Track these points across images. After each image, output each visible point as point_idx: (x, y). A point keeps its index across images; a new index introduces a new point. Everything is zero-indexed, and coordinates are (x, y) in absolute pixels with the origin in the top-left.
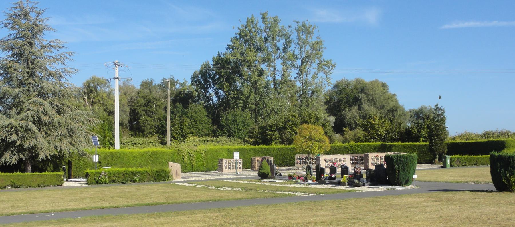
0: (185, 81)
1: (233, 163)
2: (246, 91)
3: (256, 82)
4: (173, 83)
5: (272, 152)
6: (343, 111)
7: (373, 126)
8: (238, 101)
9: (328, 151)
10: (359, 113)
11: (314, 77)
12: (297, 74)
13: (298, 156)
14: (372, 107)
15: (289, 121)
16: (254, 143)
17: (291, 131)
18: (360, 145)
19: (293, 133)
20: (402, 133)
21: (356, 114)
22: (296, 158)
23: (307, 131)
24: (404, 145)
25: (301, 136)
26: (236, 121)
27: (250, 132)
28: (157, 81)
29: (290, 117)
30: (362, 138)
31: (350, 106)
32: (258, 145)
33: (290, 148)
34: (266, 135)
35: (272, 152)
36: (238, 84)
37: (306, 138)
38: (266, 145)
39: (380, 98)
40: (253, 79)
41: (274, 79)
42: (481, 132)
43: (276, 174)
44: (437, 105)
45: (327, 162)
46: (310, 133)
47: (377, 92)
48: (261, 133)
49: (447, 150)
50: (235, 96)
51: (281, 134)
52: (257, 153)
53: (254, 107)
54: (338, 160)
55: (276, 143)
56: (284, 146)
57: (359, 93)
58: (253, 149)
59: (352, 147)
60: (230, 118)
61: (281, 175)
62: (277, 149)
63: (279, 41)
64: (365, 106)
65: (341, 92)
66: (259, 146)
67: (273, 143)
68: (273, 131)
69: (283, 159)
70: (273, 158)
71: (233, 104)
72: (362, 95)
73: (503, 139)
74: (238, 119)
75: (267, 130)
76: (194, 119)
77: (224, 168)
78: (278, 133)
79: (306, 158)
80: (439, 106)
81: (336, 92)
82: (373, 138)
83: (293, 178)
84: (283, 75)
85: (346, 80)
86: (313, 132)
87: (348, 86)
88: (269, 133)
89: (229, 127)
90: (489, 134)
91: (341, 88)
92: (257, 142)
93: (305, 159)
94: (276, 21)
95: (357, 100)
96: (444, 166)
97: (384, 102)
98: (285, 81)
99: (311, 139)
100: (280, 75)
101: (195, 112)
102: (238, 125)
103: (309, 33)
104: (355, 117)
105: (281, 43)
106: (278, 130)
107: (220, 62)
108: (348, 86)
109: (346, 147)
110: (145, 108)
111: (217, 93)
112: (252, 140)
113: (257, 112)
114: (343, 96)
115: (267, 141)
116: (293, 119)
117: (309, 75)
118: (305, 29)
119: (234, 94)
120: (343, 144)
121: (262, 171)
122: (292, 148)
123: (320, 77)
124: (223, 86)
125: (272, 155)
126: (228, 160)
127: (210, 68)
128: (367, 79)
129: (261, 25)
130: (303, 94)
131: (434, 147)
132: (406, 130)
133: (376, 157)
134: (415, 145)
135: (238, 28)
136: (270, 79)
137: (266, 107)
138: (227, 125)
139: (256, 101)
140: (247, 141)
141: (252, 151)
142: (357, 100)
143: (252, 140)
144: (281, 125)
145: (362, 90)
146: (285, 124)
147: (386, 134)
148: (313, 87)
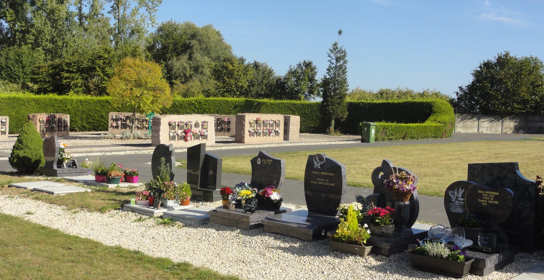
2: (38, 22)
3: (52, 12)
5: (69, 107)
6: (169, 60)
7: (231, 74)
8: (27, 36)
9: (168, 107)
10: (190, 64)
11: (135, 12)
13: (113, 115)
14: (206, 57)
15: (100, 57)
16: (38, 92)
17: (102, 75)
18: (212, 101)
19: (106, 78)
20: (271, 86)
21: (185, 65)
22: (110, 117)
23: (133, 71)
24: (279, 104)
25: (121, 79)
26: (21, 62)
27: (33, 73)
29: (102, 52)
30: (213, 90)
31: (178, 54)
32: (45, 93)
33: (99, 101)
35: (69, 107)
37: (130, 82)
38: (60, 94)
39: (215, 47)
40: (49, 7)
41: (80, 9)
42: (376, 91)
43: (60, 163)
44: (335, 44)
45: (174, 128)
46: (138, 74)
47: (212, 39)
48: (53, 76)
49: (347, 113)
50: (24, 29)
51: (86, 79)
52: (42, 107)
53: (50, 46)
54: (193, 124)
55: (77, 93)
56: (89, 97)
57: (189, 39)
58: (34, 100)
60: (12, 57)
61: (74, 164)
62: (77, 101)
64: (197, 55)
65: (167, 36)
66: (46, 96)
67: (72, 92)
68: (73, 72)
69: (87, 118)
70: (69, 116)
71: (19, 39)
72: (194, 42)
73: (428, 101)
74: (24, 59)
75: (63, 70)
78: (80, 77)
79: (127, 118)
80: (339, 46)
81: (161, 36)
82: (230, 92)
83: (110, 180)
84: (92, 6)
85: (173, 22)
86: (144, 73)
87: (175, 30)
88: (66, 75)
89: (11, 70)
90: (387, 94)
91: (166, 32)
92: (45, 89)
93: (126, 121)
95: (186, 48)
96: (365, 140)
97: (221, 52)
98: (95, 14)
99: (139, 84)
100: (89, 6)
102: (23, 67)
104: (185, 69)
106: (81, 71)
108: (175, 30)
109: (190, 104)
112: (36, 87)
113: (53, 53)
114: (169, 41)
115: (61, 89)
116: (106, 56)
117: (127, 9)
119: (21, 26)
120: (184, 99)
121: (21, 154)
122: (103, 101)
123: (141, 14)
124: (5, 14)
125: (64, 112)
128: (199, 24)
130: (119, 33)
131: (330, 107)
132: (277, 82)
133: (257, 122)
134: (294, 104)
136: (73, 9)
137: (66, 46)
138: (8, 67)
140: (28, 88)
142: (186, 48)
143: (36, 87)
144: (86, 64)
145: (193, 36)
146: (93, 62)
147: (249, 86)
148: (133, 25)
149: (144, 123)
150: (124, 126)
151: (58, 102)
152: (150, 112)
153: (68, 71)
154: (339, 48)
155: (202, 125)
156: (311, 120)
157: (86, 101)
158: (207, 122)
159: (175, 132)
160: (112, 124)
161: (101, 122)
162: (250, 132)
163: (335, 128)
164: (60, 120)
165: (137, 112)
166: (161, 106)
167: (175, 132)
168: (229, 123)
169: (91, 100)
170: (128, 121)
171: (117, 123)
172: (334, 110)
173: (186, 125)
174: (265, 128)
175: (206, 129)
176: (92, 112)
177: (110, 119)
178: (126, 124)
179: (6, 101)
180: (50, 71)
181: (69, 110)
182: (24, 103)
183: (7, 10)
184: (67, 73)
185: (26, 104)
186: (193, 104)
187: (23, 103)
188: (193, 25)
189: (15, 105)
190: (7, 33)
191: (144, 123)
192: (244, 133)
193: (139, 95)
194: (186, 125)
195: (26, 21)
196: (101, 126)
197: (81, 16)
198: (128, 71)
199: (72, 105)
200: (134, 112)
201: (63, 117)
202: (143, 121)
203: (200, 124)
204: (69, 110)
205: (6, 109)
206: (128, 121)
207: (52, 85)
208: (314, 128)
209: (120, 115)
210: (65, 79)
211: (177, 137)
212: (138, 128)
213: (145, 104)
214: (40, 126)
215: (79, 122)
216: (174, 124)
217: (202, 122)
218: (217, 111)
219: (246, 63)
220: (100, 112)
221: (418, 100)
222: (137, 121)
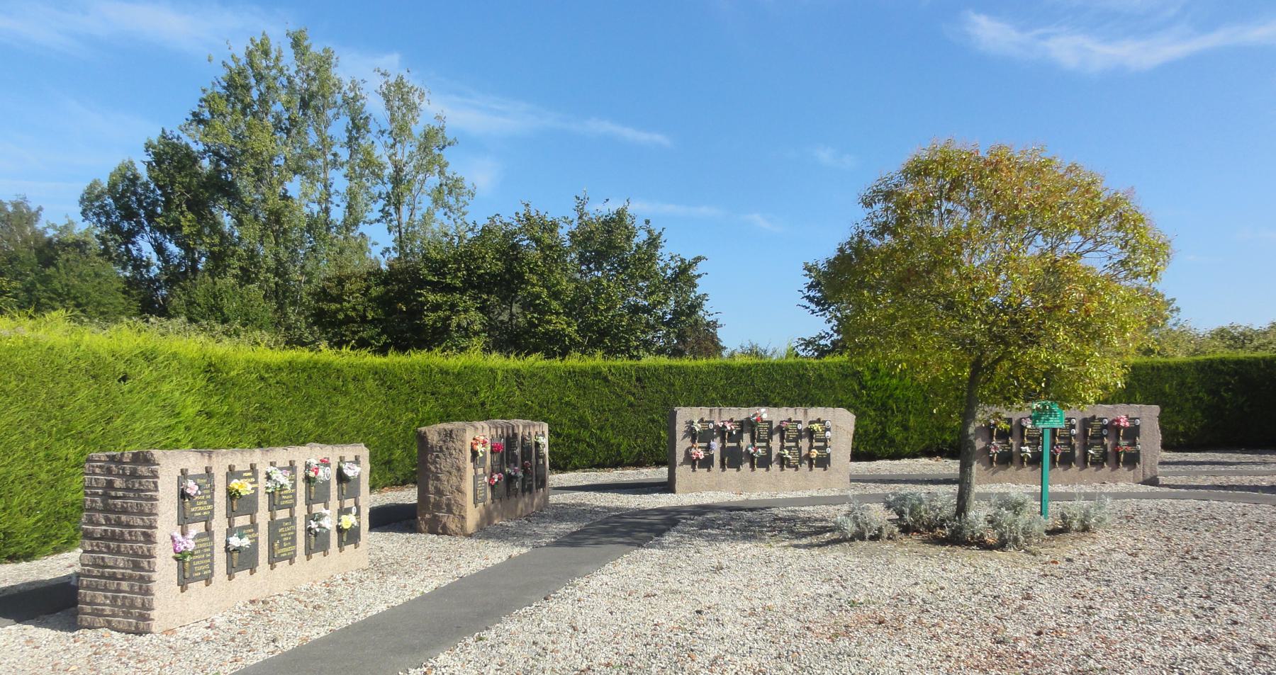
0: (71, 223)
1: (276, 499)
4: (32, 217)
13: (687, 415)
22: (680, 428)
26: (221, 310)
36: (227, 221)
53: (273, 279)
58: (375, 371)
60: (201, 301)
63: (336, 116)
76: (75, 298)
77: (164, 569)
100: (344, 205)
101: (79, 276)
105: (338, 129)
106: (478, 284)
107: (170, 158)
111: (160, 249)
126: (221, 462)
127: (136, 177)
129: (289, 61)
135: (224, 64)
139: (278, 260)
141: (370, 384)
144: (492, 265)
149: (804, 443)
151: (451, 378)
156: (1178, 412)
161: (578, 441)
168: (1133, 433)
170: (746, 437)
171: (708, 448)
179: (284, 376)
183: (182, 213)
184: (434, 291)
185: (351, 386)
189: (314, 391)
190: (179, 265)
191: (804, 443)
199: (492, 387)
205: (285, 409)
208: (1184, 435)
214: (476, 477)
220: (575, 407)
221: (1222, 352)
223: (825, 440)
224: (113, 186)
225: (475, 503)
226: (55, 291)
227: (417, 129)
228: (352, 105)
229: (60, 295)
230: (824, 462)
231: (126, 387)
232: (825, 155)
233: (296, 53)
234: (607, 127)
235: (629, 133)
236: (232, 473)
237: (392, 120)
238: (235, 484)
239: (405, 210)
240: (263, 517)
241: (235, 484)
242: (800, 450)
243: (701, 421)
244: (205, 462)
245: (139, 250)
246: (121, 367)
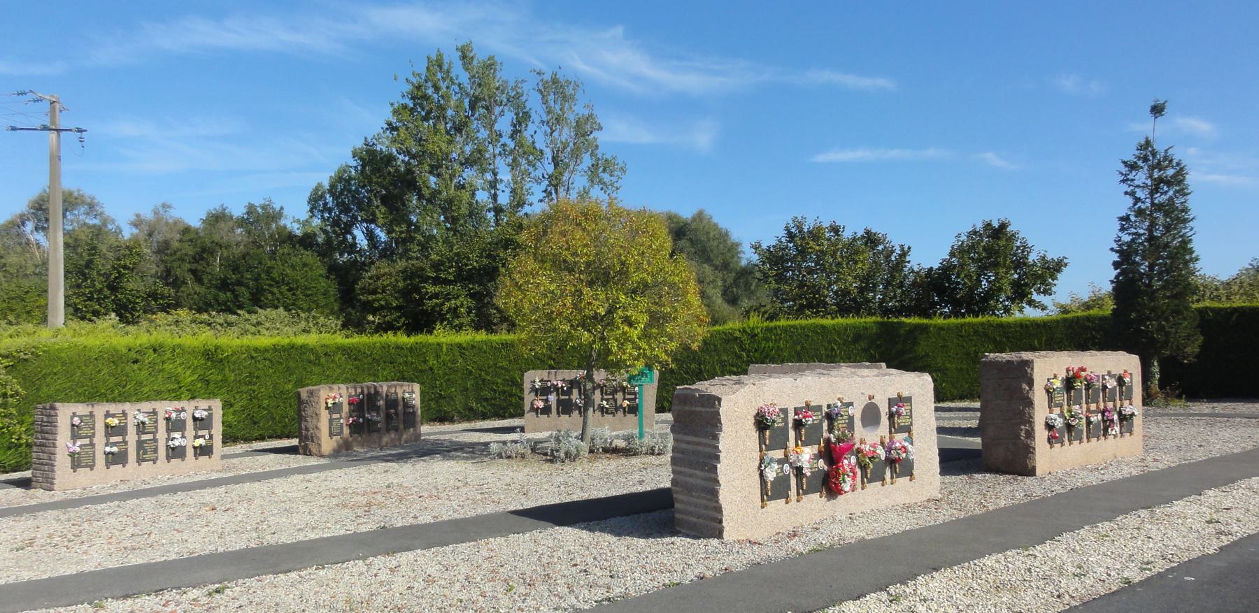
1: (141, 427)
4: (278, 215)
12: (545, 191)
13: (534, 377)
18: (785, 329)
22: (527, 386)
28: (238, 211)
34: (420, 302)
48: (406, 293)
54: (856, 412)
59: (754, 336)
62: (451, 347)
63: (502, 114)
69: (478, 389)
70: (417, 387)
75: (426, 279)
79: (573, 384)
80: (1160, 147)
82: (815, 305)
88: (432, 289)
93: (569, 392)
94: (490, 65)
100: (508, 190)
103: (565, 98)
105: (504, 124)
106: (464, 277)
107: (372, 160)
110: (194, 266)
115: (420, 321)
118: (557, 88)
147: (861, 290)
149: (619, 396)
150: (566, 407)
152: (640, 365)
153: (437, 281)
154: (1160, 156)
155: (891, 416)
157: (473, 347)
158: (909, 400)
159: (786, 459)
160: (532, 404)
161: (511, 395)
162: (1050, 427)
163: (1162, 386)
164: (392, 403)
165: (598, 369)
166: (673, 346)
167: (786, 459)
169: (485, 343)
170: (575, 391)
171: (547, 401)
172: (1167, 334)
173: (830, 417)
174: (1093, 407)
175: (908, 429)
176: (487, 374)
177: (526, 391)
178: (570, 400)
179: (268, 355)
180: (401, 284)
181: (431, 369)
182: (318, 357)
184: (434, 284)
185: (323, 360)
186: (736, 338)
187: (312, 358)
188: (675, 216)
189: (292, 364)
191: (619, 396)
192: (1030, 434)
193: (602, 311)
194: (830, 417)
195: (410, 223)
196: (511, 404)
197: (498, 210)
198: (563, 234)
199: (438, 356)
200: (589, 368)
201: (399, 391)
202: (615, 391)
203: (884, 410)
204: (431, 369)
206: (575, 391)
207: (403, 315)
209: (552, 377)
210: (430, 299)
211: (793, 481)
212: (603, 410)
213: (624, 340)
214: (331, 421)
215: (459, 399)
216: (779, 424)
217: (891, 402)
218: (798, 354)
219: (847, 235)
222: (598, 392)
223: (635, 394)
224: (333, 186)
225: (331, 435)
226: (273, 279)
227: (571, 118)
228: (516, 101)
229: (277, 282)
230: (633, 410)
231: (136, 367)
232: (1069, 83)
233: (464, 64)
234: (828, 76)
235: (851, 81)
236: (108, 415)
237: (549, 112)
238: (109, 420)
239: (562, 191)
240: (132, 437)
241: (109, 420)
242: (616, 401)
243: (541, 381)
244: (90, 409)
245: (354, 238)
246: (133, 355)
